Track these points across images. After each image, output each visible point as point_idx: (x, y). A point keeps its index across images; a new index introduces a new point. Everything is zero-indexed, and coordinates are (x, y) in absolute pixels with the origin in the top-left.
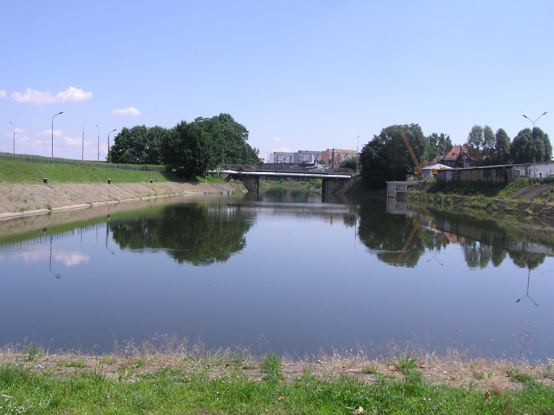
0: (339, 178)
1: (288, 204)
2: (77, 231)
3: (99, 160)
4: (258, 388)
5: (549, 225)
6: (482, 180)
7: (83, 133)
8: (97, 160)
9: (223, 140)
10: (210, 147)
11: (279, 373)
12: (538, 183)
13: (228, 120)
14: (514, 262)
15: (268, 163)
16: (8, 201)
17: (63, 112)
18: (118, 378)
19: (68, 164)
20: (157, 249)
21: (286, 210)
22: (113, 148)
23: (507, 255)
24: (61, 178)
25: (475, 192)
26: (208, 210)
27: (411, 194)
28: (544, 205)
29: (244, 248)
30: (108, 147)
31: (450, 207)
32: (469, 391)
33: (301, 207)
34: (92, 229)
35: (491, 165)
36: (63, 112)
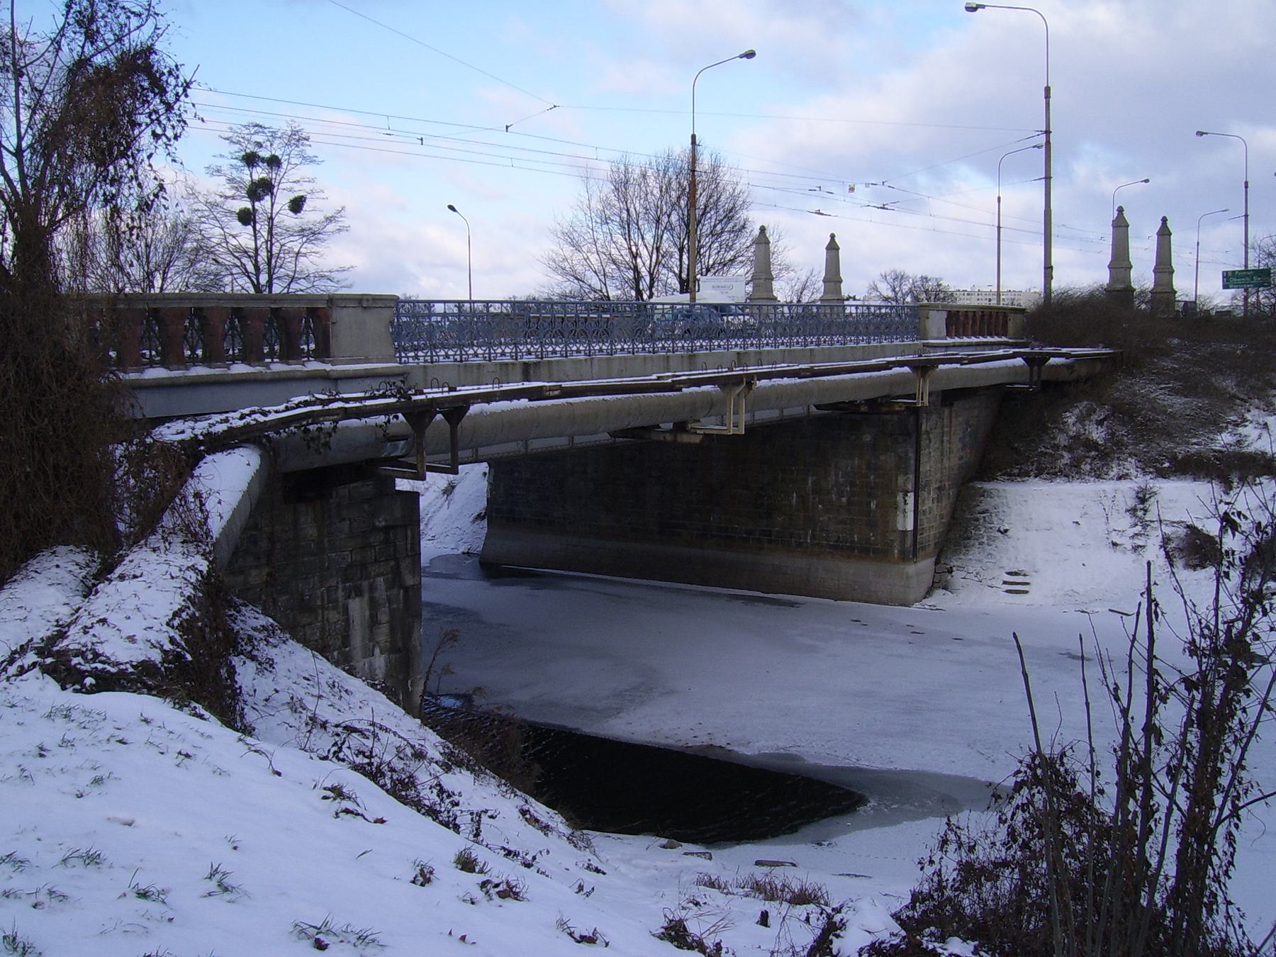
0: (367, 361)
1: (780, 596)
2: (1249, 263)
3: (473, 299)
4: (987, 547)
5: (53, 245)
6: (1176, 295)
7: (1047, 90)
8: (468, 299)
9: (1231, 728)
10: (656, 311)
11: (196, 276)
12: (928, 947)
13: (241, 578)
14: (1195, 480)
15: (523, 450)
16: (1172, 406)
17: (1080, 635)
18: (924, 437)
19: (176, 534)
20: (698, 754)
21: (397, 372)
22: (696, 941)
23: (216, 526)
24: (1085, 383)
25: (103, 564)
26: (610, 295)
27: (19, 559)
28: (1261, 507)
29: (1210, 484)
30: (1008, 381)
31: (248, 151)
32: (164, 98)
33: (782, 374)
34: (322, 195)
35: (117, 689)
36: (1080, 635)
